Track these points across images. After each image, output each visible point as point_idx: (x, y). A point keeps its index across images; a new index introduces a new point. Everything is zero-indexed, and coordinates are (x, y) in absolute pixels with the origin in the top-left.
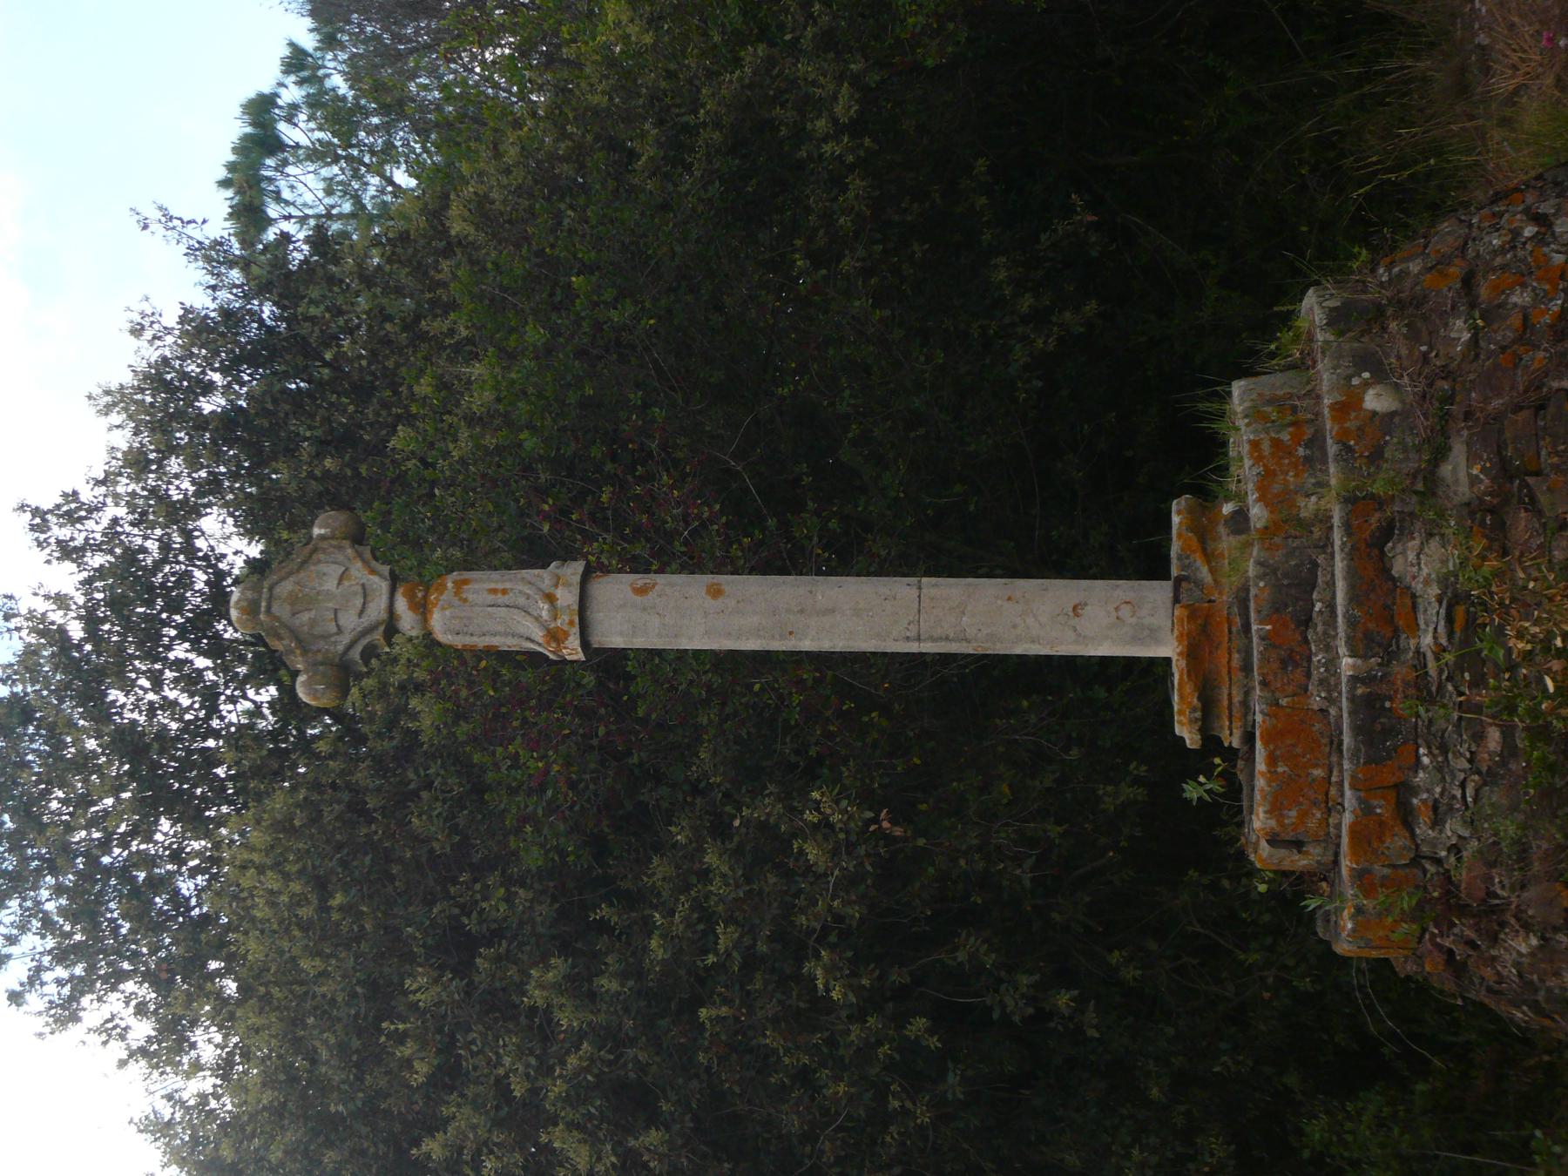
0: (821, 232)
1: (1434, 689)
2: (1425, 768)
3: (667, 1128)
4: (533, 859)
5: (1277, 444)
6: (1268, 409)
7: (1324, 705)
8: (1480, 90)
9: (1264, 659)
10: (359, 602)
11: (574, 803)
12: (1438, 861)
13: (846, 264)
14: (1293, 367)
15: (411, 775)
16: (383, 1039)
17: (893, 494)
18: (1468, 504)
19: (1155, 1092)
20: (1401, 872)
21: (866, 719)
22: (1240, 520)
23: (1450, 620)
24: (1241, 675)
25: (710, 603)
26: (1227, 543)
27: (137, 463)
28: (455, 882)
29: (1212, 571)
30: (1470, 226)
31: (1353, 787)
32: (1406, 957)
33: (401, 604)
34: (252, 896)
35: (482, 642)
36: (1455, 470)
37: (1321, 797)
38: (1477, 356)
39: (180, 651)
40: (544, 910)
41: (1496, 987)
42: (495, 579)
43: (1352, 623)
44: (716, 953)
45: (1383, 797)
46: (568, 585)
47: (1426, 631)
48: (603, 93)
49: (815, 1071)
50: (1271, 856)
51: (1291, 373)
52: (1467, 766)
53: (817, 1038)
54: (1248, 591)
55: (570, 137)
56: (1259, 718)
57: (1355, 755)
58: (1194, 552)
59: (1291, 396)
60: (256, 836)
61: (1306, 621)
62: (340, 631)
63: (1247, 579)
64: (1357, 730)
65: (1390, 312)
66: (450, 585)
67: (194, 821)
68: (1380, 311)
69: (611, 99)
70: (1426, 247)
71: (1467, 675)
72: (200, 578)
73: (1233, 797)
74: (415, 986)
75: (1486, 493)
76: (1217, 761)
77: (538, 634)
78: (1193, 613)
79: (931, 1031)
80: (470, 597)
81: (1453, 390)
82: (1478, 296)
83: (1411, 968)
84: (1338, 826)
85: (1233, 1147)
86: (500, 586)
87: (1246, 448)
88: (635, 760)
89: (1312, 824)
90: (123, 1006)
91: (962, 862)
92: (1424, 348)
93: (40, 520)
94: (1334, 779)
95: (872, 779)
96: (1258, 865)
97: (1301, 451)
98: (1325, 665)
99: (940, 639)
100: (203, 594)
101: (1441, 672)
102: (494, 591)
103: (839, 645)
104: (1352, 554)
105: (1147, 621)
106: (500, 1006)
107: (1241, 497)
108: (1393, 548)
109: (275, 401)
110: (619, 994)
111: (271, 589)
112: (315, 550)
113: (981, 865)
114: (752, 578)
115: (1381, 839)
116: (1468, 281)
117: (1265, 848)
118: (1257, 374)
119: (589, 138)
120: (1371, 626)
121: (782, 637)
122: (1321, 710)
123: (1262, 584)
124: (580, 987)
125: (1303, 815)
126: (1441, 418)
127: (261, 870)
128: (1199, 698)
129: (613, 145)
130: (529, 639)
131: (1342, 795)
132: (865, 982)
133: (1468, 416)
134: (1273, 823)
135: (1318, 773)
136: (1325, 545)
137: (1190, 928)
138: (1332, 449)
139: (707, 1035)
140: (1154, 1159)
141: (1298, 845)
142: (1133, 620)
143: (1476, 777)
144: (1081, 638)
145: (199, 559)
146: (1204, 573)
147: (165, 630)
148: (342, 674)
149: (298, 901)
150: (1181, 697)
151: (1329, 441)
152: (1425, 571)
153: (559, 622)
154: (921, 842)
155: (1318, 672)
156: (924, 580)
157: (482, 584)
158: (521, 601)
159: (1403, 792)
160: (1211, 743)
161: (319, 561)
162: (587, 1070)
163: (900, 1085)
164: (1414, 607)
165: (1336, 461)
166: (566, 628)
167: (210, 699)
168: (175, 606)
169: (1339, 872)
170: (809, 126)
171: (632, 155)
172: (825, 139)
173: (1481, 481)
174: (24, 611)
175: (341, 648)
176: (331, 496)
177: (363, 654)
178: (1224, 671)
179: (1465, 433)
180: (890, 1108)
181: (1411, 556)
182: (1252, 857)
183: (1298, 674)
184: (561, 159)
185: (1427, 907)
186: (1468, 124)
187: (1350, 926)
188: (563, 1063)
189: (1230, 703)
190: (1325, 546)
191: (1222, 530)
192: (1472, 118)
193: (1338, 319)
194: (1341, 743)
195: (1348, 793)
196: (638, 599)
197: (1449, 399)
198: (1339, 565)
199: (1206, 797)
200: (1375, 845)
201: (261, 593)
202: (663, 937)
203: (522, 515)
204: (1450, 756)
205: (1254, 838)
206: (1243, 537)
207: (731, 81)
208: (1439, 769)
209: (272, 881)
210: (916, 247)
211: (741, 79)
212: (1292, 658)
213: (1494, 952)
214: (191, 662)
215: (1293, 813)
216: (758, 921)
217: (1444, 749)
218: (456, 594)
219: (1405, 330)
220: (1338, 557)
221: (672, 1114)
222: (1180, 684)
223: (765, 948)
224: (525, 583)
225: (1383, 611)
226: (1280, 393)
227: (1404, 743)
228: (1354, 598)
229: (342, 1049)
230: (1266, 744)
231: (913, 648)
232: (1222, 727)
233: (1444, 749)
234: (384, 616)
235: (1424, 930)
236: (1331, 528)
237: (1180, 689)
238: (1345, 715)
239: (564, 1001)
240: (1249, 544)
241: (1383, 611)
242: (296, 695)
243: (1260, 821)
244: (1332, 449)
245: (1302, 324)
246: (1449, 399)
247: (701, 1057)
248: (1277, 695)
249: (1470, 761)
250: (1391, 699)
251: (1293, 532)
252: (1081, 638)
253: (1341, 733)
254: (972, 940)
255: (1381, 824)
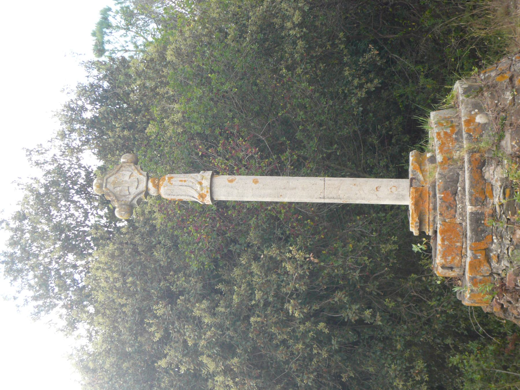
0: (290, 59)
1: (498, 217)
2: (495, 243)
3: (240, 358)
4: (194, 266)
5: (446, 133)
6: (443, 122)
7: (461, 222)
8: (513, 14)
9: (441, 206)
10: (136, 184)
11: (209, 248)
12: (499, 275)
13: (299, 71)
14: (451, 107)
15: (154, 240)
16: (145, 325)
17: (313, 149)
18: (511, 155)
19: (399, 347)
20: (486, 278)
21: (306, 222)
22: (433, 159)
23: (504, 193)
24: (433, 211)
25: (253, 185)
26: (428, 166)
27: (63, 135)
28: (168, 275)
29: (423, 176)
30: (512, 60)
31: (471, 249)
32: (487, 306)
33: (150, 185)
34: (100, 279)
35: (177, 198)
36: (506, 143)
37: (459, 253)
38: (514, 104)
39: (76, 198)
40: (199, 285)
41: (518, 317)
42: (182, 177)
43: (471, 194)
44: (255, 301)
45: (481, 253)
46: (206, 179)
47: (496, 197)
48: (217, 13)
49: (287, 341)
50: (442, 272)
51: (450, 110)
52: (509, 243)
53: (289, 329)
54: (435, 183)
55: (207, 28)
56: (439, 226)
57: (471, 238)
58: (417, 169)
59: (451, 117)
60: (103, 259)
61: (455, 194)
62: (130, 194)
63: (435, 179)
64: (472, 230)
65: (485, 89)
66: (167, 179)
67: (81, 255)
68: (481, 89)
69: (219, 15)
70: (497, 67)
71: (510, 212)
72: (83, 174)
73: (429, 252)
74: (157, 308)
75: (517, 151)
76: (424, 239)
77: (196, 195)
78: (417, 190)
79: (326, 327)
80: (174, 183)
81: (506, 115)
82: (515, 84)
83: (488, 310)
84: (465, 262)
85: (426, 364)
86: (183, 179)
87: (435, 135)
88: (229, 235)
89: (456, 261)
90: (58, 315)
91: (336, 271)
92: (496, 102)
93: (30, 152)
94: (464, 247)
95: (307, 242)
96: (438, 275)
97: (454, 136)
98: (461, 208)
99: (331, 198)
100: (84, 179)
101: (501, 211)
102: (181, 181)
103: (297, 200)
104: (471, 171)
105: (401, 193)
106: (184, 316)
107: (433, 151)
108: (485, 169)
109: (108, 114)
110: (224, 312)
111: (107, 180)
112: (122, 166)
113: (342, 272)
114: (268, 177)
115: (480, 267)
116: (511, 79)
117: (440, 269)
118: (439, 110)
119: (214, 28)
120: (477, 195)
121: (278, 197)
122: (460, 223)
123: (440, 181)
124: (212, 311)
125: (453, 259)
126: (502, 125)
127: (104, 270)
128: (418, 219)
129: (221, 30)
130: (193, 197)
131: (467, 252)
132: (305, 311)
133: (511, 125)
134: (443, 261)
135: (459, 244)
136: (462, 168)
137: (412, 294)
138: (465, 135)
139: (252, 327)
140: (399, 368)
141: (451, 268)
142: (396, 192)
143: (512, 247)
144: (378, 198)
145: (82, 167)
146: (421, 177)
147: (71, 191)
148: (130, 207)
149: (116, 280)
150: (413, 218)
151: (464, 133)
152: (496, 177)
153: (203, 191)
154: (322, 264)
155: (459, 211)
156: (326, 178)
157: (178, 178)
158: (191, 184)
159: (487, 251)
160: (422, 234)
161: (123, 170)
162: (213, 337)
163: (317, 345)
164: (492, 189)
165: (466, 139)
166: (205, 193)
167: (86, 214)
168: (74, 183)
169: (465, 278)
170: (285, 25)
171: (227, 34)
172: (290, 29)
173: (515, 147)
174: (25, 183)
175: (130, 200)
176: (126, 148)
177: (137, 202)
178: (427, 210)
179: (510, 130)
180: (314, 353)
181: (491, 172)
182: (436, 272)
183: (453, 211)
184: (203, 35)
185: (495, 290)
186: (510, 25)
187: (468, 296)
188: (205, 334)
189: (429, 220)
190: (462, 168)
191: (427, 162)
192: (511, 23)
193: (467, 92)
194: (466, 235)
195: (469, 252)
196: (230, 184)
197: (505, 119)
198: (467, 175)
199: (420, 251)
200: (478, 269)
201: (103, 181)
202: (238, 294)
203: (189, 154)
204: (504, 239)
205: (436, 266)
206: (434, 165)
207: (259, 10)
208: (500, 244)
209: (108, 273)
210: (321, 65)
211: (262, 9)
212: (450, 206)
213: (517, 305)
214: (80, 202)
215: (450, 258)
216: (268, 290)
217: (502, 237)
218: (169, 182)
219: (490, 96)
220: (466, 172)
221: (241, 354)
222: (412, 214)
223: (271, 299)
224: (193, 178)
225: (481, 190)
226: (447, 116)
227: (488, 235)
228: (472, 186)
229: (130, 330)
230: (441, 234)
231: (322, 201)
232: (426, 229)
233: (502, 237)
234: (145, 189)
235: (493, 297)
236: (464, 162)
237: (412, 216)
238: (468, 225)
239: (206, 315)
240: (436, 167)
241: (481, 190)
242: (114, 214)
243: (438, 260)
244: (465, 135)
245: (454, 92)
246: (505, 119)
247: (250, 335)
248: (445, 218)
249: (511, 241)
250: (484, 220)
251: (451, 163)
252: (378, 198)
253: (467, 231)
254: (339, 294)
255: (480, 262)
